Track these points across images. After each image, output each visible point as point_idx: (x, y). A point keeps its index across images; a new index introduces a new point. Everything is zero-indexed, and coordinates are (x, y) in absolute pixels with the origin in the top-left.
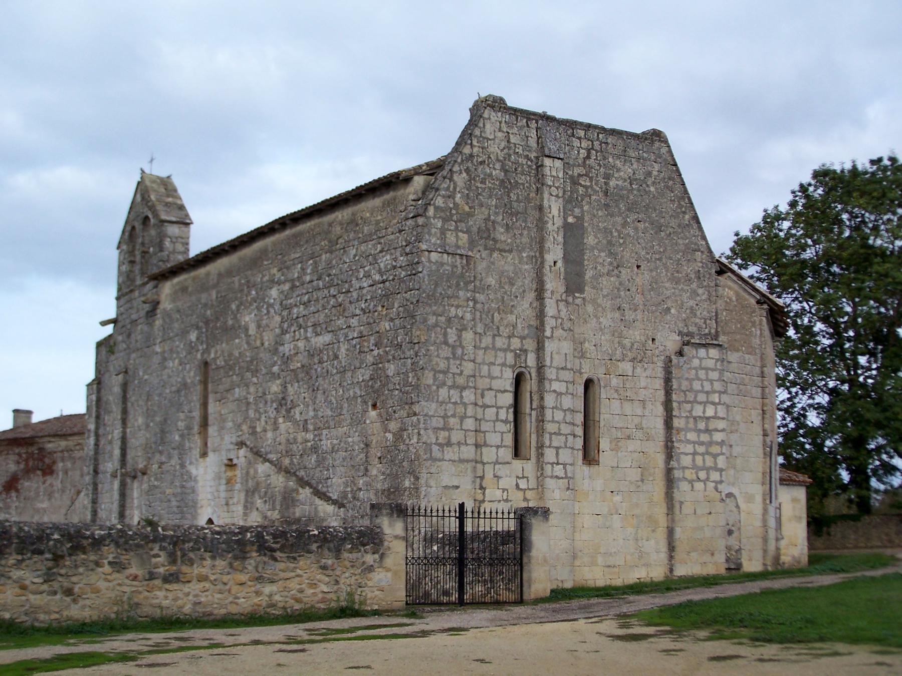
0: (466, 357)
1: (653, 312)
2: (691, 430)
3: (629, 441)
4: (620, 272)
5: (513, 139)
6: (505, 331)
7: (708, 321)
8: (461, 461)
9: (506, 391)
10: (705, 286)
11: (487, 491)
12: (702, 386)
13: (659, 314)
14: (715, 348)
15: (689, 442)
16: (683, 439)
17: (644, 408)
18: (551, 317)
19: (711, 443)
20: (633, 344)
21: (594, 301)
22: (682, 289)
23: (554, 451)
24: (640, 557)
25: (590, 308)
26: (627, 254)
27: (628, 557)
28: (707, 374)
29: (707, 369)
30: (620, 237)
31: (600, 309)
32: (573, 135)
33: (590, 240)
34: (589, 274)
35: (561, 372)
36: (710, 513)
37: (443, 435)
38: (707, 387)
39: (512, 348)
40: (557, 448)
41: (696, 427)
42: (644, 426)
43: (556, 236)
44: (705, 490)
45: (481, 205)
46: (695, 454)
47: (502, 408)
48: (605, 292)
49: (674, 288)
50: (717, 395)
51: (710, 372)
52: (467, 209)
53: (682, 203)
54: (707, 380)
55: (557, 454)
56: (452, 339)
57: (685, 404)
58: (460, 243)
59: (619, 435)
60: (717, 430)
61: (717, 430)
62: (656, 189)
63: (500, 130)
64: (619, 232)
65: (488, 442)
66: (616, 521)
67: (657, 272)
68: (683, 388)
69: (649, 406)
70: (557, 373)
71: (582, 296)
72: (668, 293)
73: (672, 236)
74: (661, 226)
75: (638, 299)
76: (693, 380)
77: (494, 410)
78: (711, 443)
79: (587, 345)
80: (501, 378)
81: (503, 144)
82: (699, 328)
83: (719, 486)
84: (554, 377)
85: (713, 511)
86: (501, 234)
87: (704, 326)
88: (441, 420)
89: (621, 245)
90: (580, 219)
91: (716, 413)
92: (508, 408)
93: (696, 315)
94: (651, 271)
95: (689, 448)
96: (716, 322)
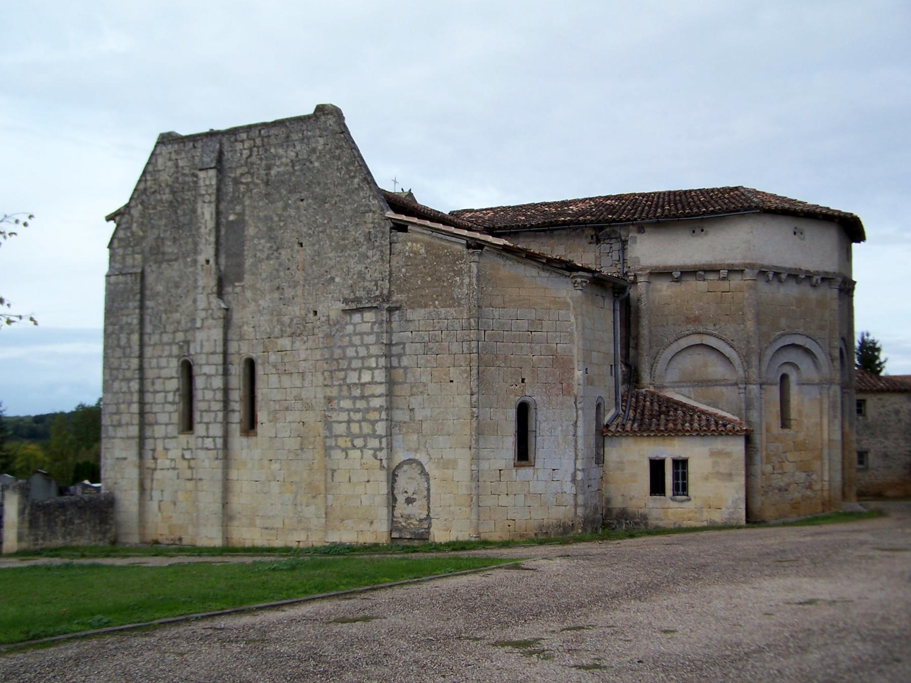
0: (133, 355)
1: (314, 285)
2: (344, 398)
3: (287, 413)
4: (280, 254)
5: (181, 163)
6: (170, 328)
7: (380, 283)
8: (129, 438)
9: (172, 378)
10: (378, 247)
11: (159, 461)
12: (357, 352)
13: (321, 285)
14: (370, 311)
15: (342, 410)
16: (336, 407)
17: (303, 380)
18: (203, 310)
19: (368, 410)
20: (292, 320)
21: (253, 287)
22: (349, 255)
23: (204, 426)
24: (300, 521)
25: (249, 294)
26: (287, 236)
27: (287, 521)
28: (362, 339)
29: (362, 334)
30: (280, 220)
31: (259, 292)
32: (236, 141)
33: (251, 231)
34: (248, 262)
35: (211, 356)
36: (368, 481)
37: (116, 418)
38: (363, 352)
39: (177, 341)
40: (207, 424)
41: (351, 394)
42: (303, 397)
43: (207, 237)
44: (362, 458)
45: (153, 227)
46: (349, 422)
47: (169, 392)
48: (264, 276)
49: (339, 257)
50: (374, 359)
51: (365, 337)
52: (141, 234)
53: (352, 168)
54: (362, 344)
55: (207, 429)
56: (123, 342)
57: (337, 373)
58: (136, 263)
59: (277, 407)
60: (373, 396)
61: (373, 396)
62: (322, 163)
63: (170, 159)
64: (280, 216)
65: (158, 421)
66: (275, 487)
67: (320, 245)
68: (336, 356)
69: (309, 377)
70: (207, 358)
71: (241, 284)
72: (332, 263)
73: (338, 205)
74: (326, 199)
75: (299, 276)
76: (347, 346)
77: (163, 394)
78: (368, 410)
79: (245, 328)
80: (167, 367)
81: (172, 170)
82: (369, 292)
83: (378, 453)
84: (204, 362)
85: (372, 479)
86: (169, 248)
87: (375, 288)
88: (115, 407)
89: (281, 228)
90: (241, 215)
91: (373, 378)
92: (175, 392)
93: (364, 278)
94: (314, 245)
95: (344, 416)
96: (390, 282)
